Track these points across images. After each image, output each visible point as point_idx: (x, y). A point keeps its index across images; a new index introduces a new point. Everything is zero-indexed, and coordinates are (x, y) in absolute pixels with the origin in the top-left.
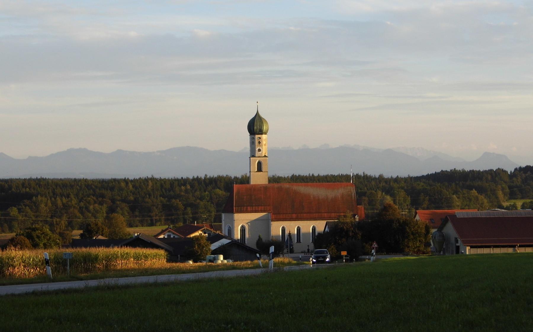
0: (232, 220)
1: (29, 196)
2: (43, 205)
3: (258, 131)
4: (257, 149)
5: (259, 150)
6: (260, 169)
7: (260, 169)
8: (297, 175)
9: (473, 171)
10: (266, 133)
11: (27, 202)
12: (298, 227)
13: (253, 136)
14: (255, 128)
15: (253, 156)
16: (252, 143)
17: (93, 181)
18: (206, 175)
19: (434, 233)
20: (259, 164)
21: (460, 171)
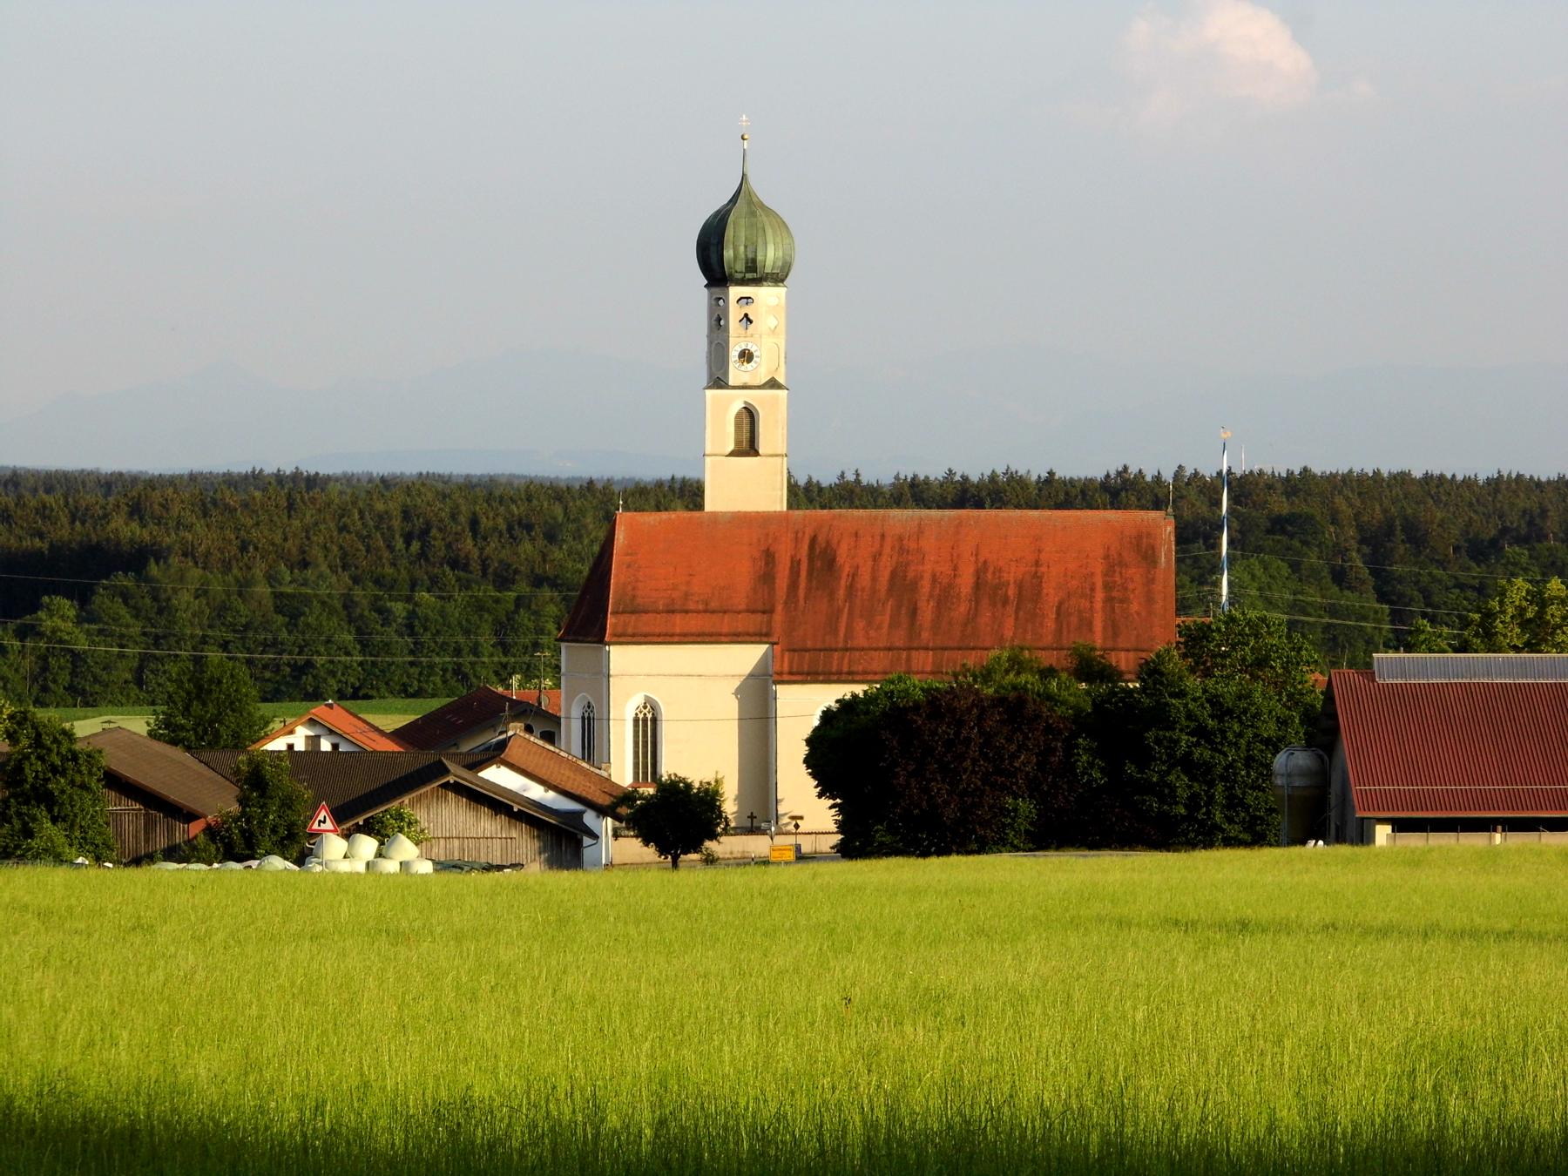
0: (602, 675)
1: (137, 559)
2: (185, 597)
3: (740, 266)
4: (734, 354)
5: (746, 356)
6: (748, 446)
7: (748, 446)
8: (1460, 477)
9: (121, 474)
10: (778, 279)
11: (125, 581)
12: (651, 705)
13: (717, 291)
14: (728, 254)
15: (719, 381)
16: (718, 322)
17: (232, 481)
18: (1051, 473)
19: (121, 699)
20: (749, 416)
21: (1290, 473)
